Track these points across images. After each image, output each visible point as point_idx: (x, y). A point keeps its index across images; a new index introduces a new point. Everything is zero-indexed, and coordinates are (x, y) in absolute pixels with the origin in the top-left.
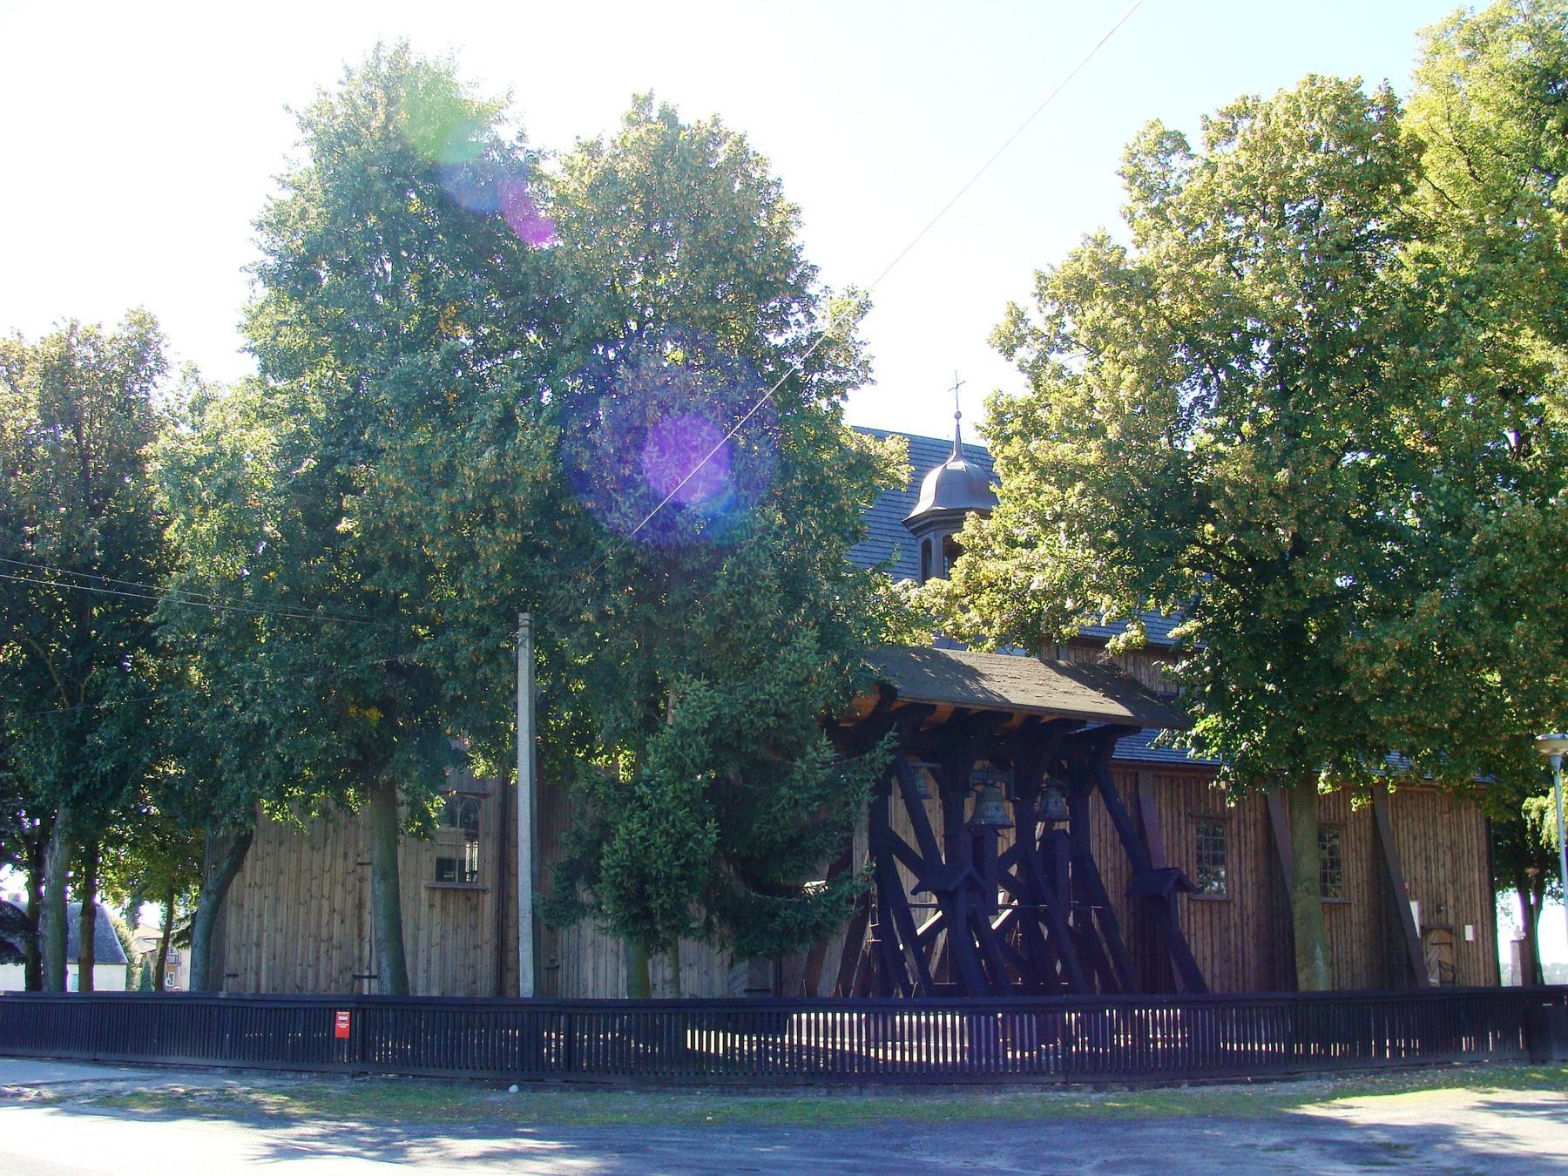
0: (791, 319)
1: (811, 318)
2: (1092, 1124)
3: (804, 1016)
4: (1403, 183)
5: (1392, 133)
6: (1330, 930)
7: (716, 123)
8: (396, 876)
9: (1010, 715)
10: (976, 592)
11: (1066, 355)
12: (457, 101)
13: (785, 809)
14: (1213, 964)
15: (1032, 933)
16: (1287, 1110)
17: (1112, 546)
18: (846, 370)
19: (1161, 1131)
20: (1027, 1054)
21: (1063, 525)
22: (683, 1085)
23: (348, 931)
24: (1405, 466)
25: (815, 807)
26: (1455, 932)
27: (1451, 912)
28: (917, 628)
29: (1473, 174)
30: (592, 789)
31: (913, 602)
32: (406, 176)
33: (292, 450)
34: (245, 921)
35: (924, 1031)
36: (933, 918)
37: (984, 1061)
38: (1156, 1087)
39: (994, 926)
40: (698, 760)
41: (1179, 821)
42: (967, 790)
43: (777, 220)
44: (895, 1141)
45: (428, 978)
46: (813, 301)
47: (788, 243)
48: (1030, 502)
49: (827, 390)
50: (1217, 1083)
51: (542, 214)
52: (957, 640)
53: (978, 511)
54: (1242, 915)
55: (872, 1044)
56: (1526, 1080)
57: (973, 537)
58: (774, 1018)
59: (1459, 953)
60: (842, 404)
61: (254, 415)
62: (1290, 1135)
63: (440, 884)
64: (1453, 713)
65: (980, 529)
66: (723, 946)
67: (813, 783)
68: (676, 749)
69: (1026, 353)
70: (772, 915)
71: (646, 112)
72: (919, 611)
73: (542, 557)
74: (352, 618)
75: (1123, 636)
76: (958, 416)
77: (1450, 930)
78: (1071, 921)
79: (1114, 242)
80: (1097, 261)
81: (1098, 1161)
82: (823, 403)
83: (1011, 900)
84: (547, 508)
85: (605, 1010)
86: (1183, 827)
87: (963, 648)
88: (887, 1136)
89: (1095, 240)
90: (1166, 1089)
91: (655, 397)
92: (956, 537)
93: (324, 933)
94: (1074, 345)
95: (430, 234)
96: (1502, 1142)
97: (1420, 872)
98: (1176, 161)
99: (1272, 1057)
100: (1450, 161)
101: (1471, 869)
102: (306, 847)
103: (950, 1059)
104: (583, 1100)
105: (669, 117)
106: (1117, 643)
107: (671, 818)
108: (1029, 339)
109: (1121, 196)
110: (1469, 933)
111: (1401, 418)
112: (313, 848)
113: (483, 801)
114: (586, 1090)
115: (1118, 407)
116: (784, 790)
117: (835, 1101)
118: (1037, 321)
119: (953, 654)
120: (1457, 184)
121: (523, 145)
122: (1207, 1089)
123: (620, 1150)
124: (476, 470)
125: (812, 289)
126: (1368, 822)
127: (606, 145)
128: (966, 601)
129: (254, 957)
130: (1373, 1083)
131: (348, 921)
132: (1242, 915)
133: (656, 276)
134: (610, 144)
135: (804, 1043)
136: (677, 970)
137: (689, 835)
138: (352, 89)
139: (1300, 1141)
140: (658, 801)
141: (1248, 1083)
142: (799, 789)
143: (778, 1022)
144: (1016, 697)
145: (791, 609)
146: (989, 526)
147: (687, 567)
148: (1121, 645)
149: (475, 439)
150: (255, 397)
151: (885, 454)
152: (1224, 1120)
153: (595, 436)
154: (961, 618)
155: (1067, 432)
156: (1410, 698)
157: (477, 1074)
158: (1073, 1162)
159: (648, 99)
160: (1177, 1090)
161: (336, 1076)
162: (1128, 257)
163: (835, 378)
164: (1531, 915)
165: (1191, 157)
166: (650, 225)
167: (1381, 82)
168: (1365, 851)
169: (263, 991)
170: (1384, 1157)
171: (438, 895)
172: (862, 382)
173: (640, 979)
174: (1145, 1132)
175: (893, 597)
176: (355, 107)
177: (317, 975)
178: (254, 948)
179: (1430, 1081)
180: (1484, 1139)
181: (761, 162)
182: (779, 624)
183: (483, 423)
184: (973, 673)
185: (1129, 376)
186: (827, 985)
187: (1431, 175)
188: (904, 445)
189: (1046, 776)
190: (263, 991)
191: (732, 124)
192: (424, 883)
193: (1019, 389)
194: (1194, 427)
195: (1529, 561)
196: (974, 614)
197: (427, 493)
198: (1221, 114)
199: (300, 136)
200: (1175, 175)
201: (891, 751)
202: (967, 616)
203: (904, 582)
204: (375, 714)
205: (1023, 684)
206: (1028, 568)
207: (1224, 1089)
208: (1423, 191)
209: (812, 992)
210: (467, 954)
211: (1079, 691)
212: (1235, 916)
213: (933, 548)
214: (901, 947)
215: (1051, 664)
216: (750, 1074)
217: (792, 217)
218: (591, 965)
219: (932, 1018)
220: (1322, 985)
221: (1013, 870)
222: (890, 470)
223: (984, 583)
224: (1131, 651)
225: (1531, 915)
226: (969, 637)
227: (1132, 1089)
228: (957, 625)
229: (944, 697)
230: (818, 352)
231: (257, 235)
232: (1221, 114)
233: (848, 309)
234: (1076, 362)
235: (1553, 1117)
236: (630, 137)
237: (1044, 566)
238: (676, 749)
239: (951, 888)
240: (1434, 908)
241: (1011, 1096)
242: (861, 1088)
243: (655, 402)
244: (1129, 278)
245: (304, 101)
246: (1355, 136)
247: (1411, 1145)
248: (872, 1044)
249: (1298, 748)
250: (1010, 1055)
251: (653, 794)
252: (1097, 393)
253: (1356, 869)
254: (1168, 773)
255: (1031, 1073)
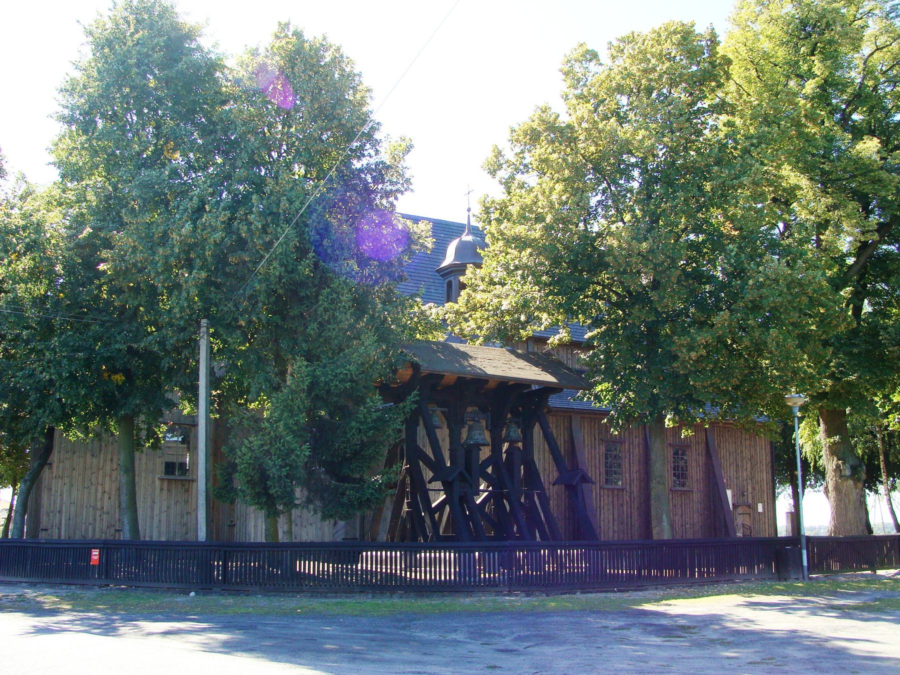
0: (366, 153)
1: (377, 152)
2: (519, 615)
3: (369, 553)
4: (718, 82)
5: (713, 54)
6: (681, 506)
7: (324, 39)
8: (133, 471)
9: (486, 381)
10: (473, 310)
11: (526, 175)
12: (177, 23)
13: (354, 434)
14: (613, 525)
15: (499, 506)
16: (636, 607)
17: (546, 284)
18: (397, 183)
19: (556, 619)
20: (492, 575)
21: (520, 272)
22: (289, 592)
23: (113, 503)
24: (717, 240)
25: (371, 433)
26: (752, 507)
27: (750, 495)
28: (436, 331)
29: (758, 77)
30: (241, 421)
31: (433, 316)
32: (147, 65)
33: (78, 223)
34: (52, 497)
35: (433, 562)
36: (443, 497)
37: (467, 579)
38: (562, 594)
39: (478, 502)
40: (302, 407)
41: (595, 443)
42: (462, 423)
43: (358, 96)
44: (403, 624)
45: (159, 531)
46: (378, 142)
47: (364, 109)
48: (501, 258)
49: (387, 194)
50: (598, 592)
51: (224, 89)
52: (462, 338)
53: (474, 264)
54: (630, 497)
55: (408, 569)
56: (773, 589)
57: (471, 279)
58: (352, 554)
59: (754, 519)
60: (395, 202)
61: (55, 203)
62: (630, 621)
63: (166, 477)
64: (735, 381)
65: (475, 275)
66: (315, 512)
67: (370, 420)
68: (288, 401)
69: (503, 174)
70: (343, 494)
71: (286, 31)
72: (437, 321)
73: (215, 287)
74: (108, 321)
75: (557, 337)
76: (469, 210)
77: (749, 506)
78: (522, 500)
79: (553, 111)
80: (543, 121)
81: (516, 635)
82: (384, 201)
83: (488, 487)
84: (221, 259)
85: (254, 548)
86: (597, 447)
87: (465, 342)
88: (400, 621)
89: (541, 109)
90: (568, 596)
91: (285, 195)
92: (462, 279)
93: (99, 506)
94: (530, 170)
95: (159, 100)
96: (748, 624)
97: (732, 472)
98: (592, 66)
99: (630, 577)
100: (747, 69)
101: (761, 471)
102: (89, 455)
103: (443, 578)
104: (230, 600)
105: (298, 35)
106: (554, 340)
107: (282, 441)
108: (504, 166)
109: (562, 85)
110: (760, 508)
111: (716, 216)
112: (93, 455)
113: (193, 429)
114: (234, 595)
115: (551, 206)
116: (353, 424)
117: (375, 601)
118: (510, 155)
119: (454, 345)
120: (750, 82)
121: (215, 50)
122: (590, 595)
123: (240, 628)
124: (181, 236)
125: (377, 136)
126: (703, 445)
127: (262, 51)
128: (467, 315)
129: (57, 519)
130: (686, 592)
131: (113, 497)
132: (630, 497)
133: (290, 127)
134: (264, 50)
135: (369, 569)
136: (291, 526)
137: (293, 451)
138: (116, 14)
139: (633, 625)
140: (274, 431)
141: (615, 592)
142: (361, 423)
143: (354, 557)
144: (490, 371)
145: (359, 318)
146: (480, 272)
147: (303, 294)
148: (556, 342)
149: (180, 219)
150: (57, 193)
151: (419, 231)
152: (594, 612)
153: (251, 217)
154: (464, 325)
155: (523, 219)
156: (712, 371)
157: (171, 585)
158: (501, 636)
159: (287, 25)
160: (573, 596)
161: (91, 588)
162: (560, 119)
163: (390, 187)
164: (796, 497)
165: (601, 64)
166: (286, 97)
167: (709, 25)
168: (702, 460)
169: (63, 538)
170: (680, 633)
171: (166, 483)
172: (406, 190)
173: (272, 531)
174: (548, 619)
175: (423, 313)
176: (117, 25)
177: (94, 529)
178: (58, 514)
179: (719, 590)
180: (738, 622)
181: (350, 62)
182: (352, 327)
183: (186, 210)
184: (465, 356)
185: (559, 187)
186: (383, 537)
187: (735, 77)
188: (430, 226)
189: (509, 416)
190: (63, 538)
191: (333, 40)
192: (158, 476)
193: (498, 194)
194: (599, 218)
195: (780, 295)
196: (472, 323)
197: (151, 249)
198: (618, 40)
199: (84, 39)
200: (591, 74)
201: (414, 402)
202: (468, 324)
203: (430, 304)
204: (119, 378)
205: (495, 363)
206: (498, 297)
207: (599, 595)
208: (731, 87)
209: (374, 539)
210: (182, 517)
211: (528, 368)
212: (626, 497)
213: (453, 287)
214: (423, 514)
215: (513, 352)
216: (328, 586)
217: (368, 94)
218: (253, 524)
219: (438, 555)
220: (666, 536)
221: (489, 470)
222: (421, 241)
223: (478, 305)
224: (562, 345)
225: (796, 497)
226: (469, 336)
227: (548, 595)
228: (461, 330)
229: (449, 370)
230: (380, 172)
231: (60, 97)
232: (618, 40)
233: (400, 148)
234: (532, 179)
235: (782, 610)
236: (276, 46)
237: (508, 295)
238: (288, 401)
239: (450, 480)
240: (740, 493)
241: (475, 599)
242: (392, 594)
243: (285, 198)
244: (561, 131)
245: (89, 20)
246: (692, 54)
247: (697, 627)
248: (408, 569)
249: (654, 401)
250: (482, 576)
251: (272, 427)
252: (540, 197)
253: (696, 472)
254: (588, 416)
255: (490, 586)
